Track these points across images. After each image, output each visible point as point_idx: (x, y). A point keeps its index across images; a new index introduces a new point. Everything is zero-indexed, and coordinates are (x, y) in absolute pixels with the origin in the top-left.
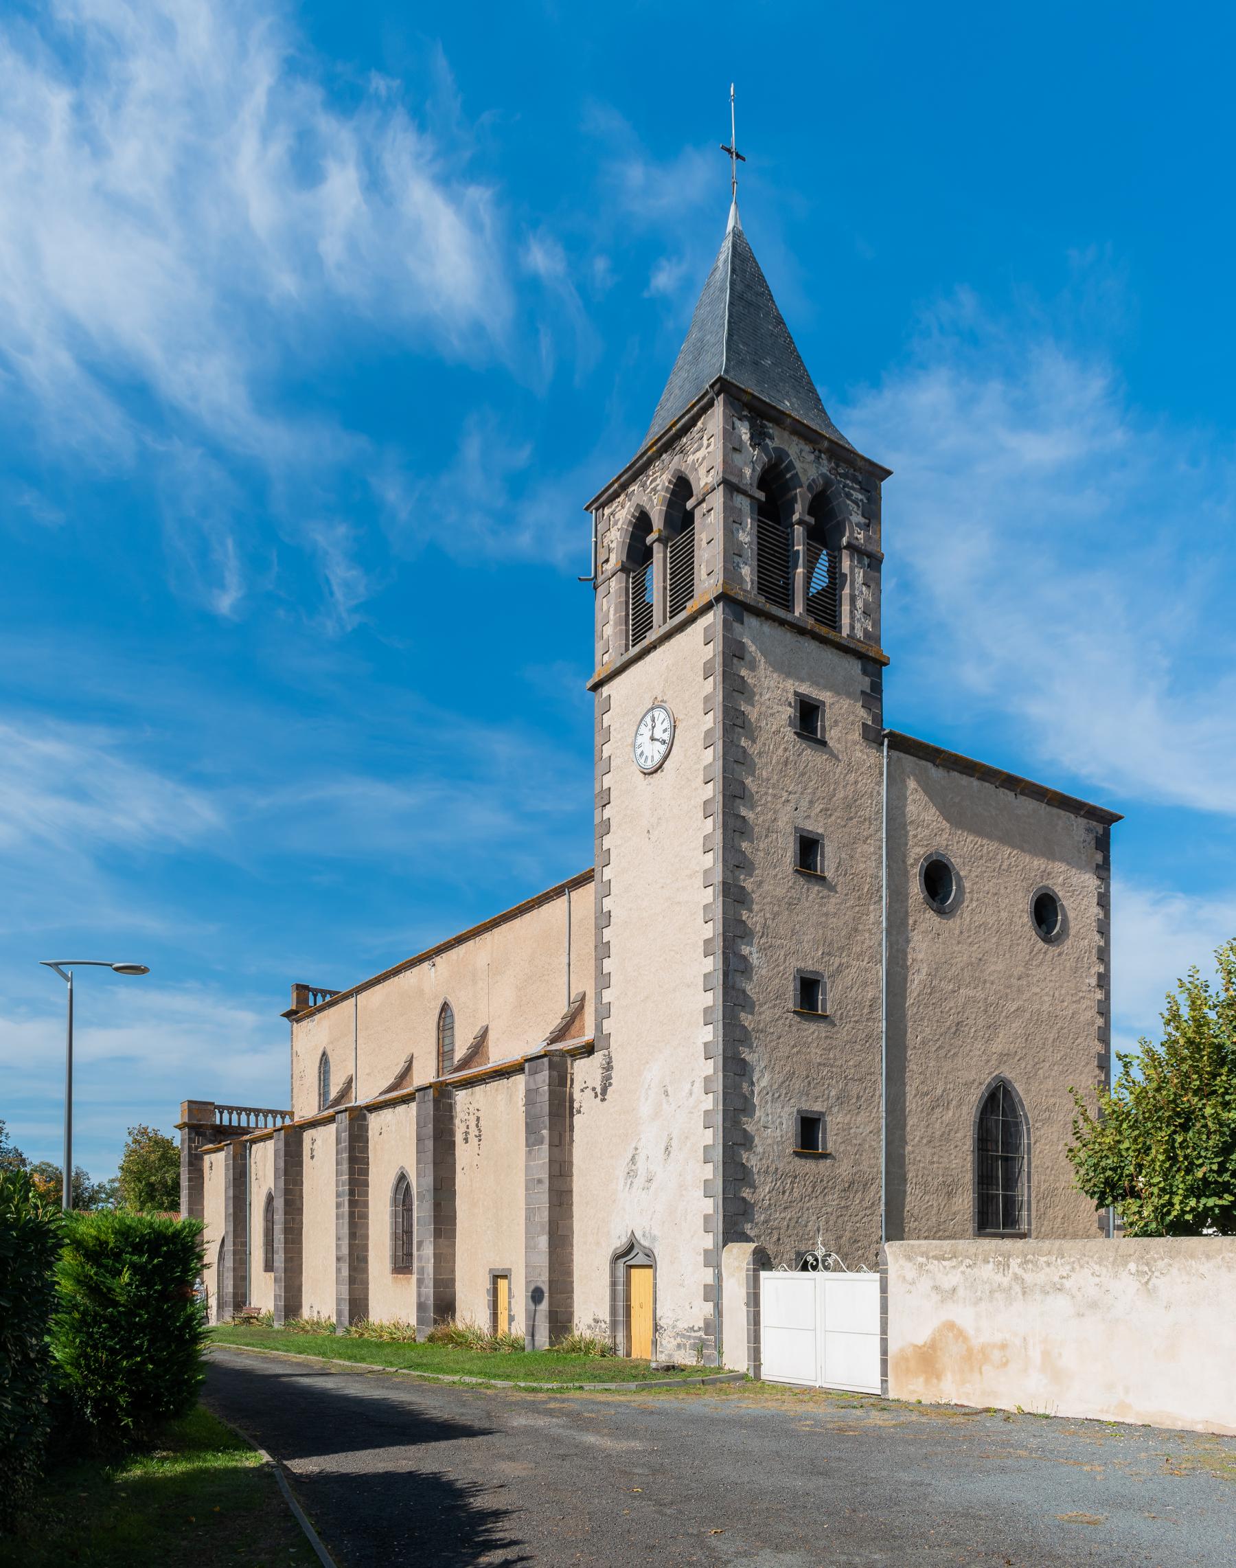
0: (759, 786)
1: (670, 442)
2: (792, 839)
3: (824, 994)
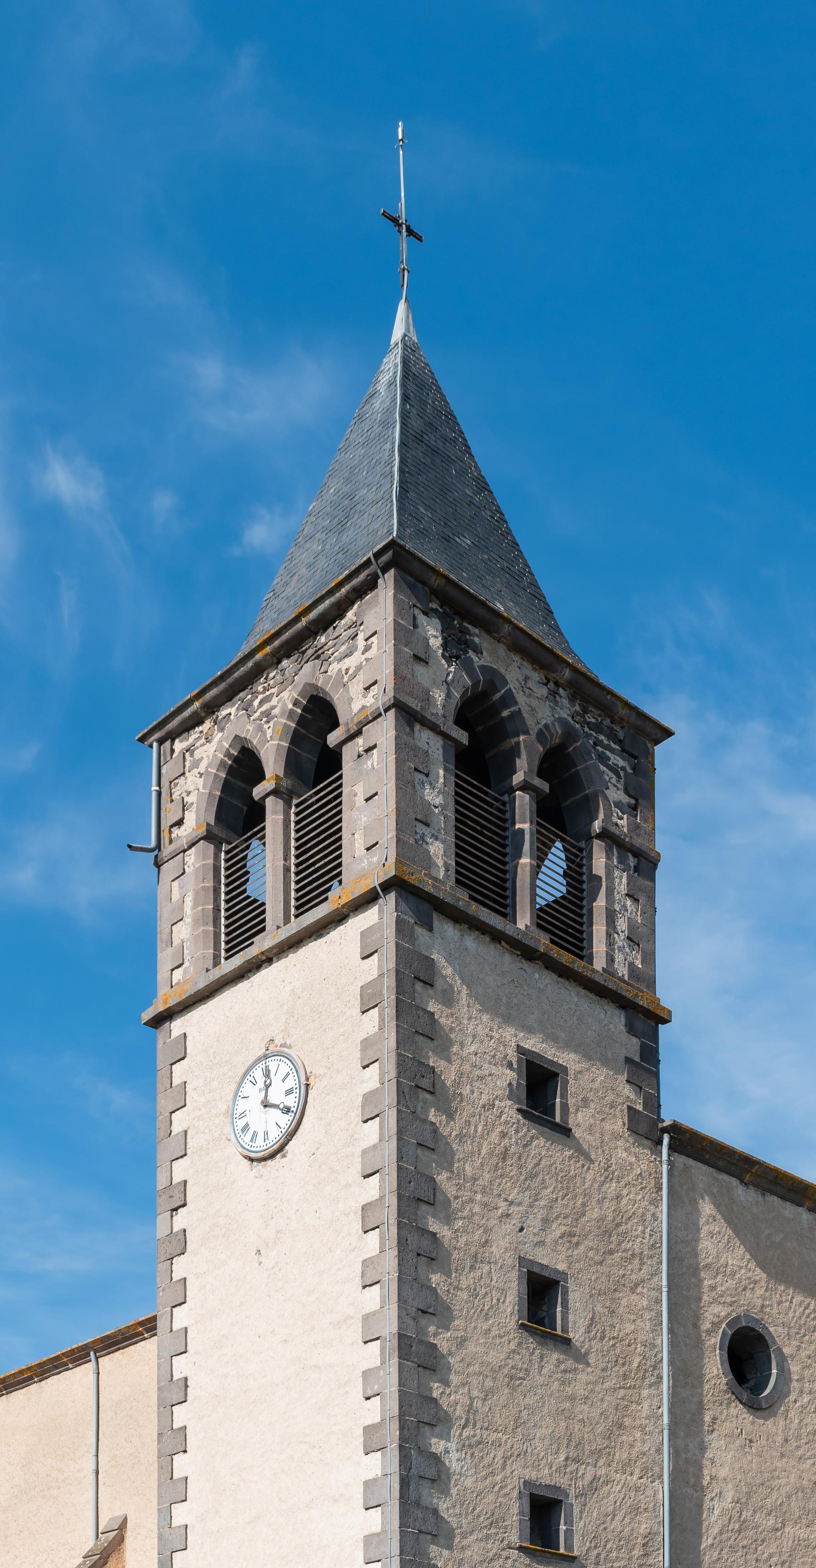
0: (460, 1187)
1: (299, 639)
2: (515, 1274)
3: (569, 1522)
